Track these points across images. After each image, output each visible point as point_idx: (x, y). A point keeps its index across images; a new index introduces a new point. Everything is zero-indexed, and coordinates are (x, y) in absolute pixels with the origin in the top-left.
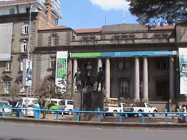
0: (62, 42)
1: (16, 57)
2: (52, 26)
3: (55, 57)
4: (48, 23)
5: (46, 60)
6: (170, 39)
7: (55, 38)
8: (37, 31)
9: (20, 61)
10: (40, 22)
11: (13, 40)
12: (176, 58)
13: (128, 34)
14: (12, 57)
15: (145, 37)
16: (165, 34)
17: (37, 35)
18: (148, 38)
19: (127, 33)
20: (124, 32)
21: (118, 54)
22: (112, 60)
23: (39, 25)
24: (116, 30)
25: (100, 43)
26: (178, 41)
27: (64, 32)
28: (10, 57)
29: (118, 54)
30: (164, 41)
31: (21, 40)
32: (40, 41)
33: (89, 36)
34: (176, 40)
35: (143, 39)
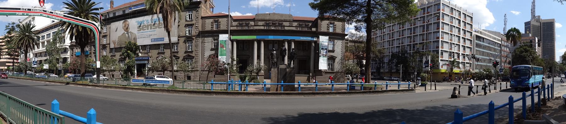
1: (182, 40)
2: (209, 13)
3: (218, 39)
5: (209, 43)
7: (216, 23)
8: (201, 18)
9: (186, 43)
10: (202, 10)
11: (179, 26)
12: (317, 44)
13: (277, 22)
14: (179, 40)
15: (291, 25)
16: (307, 24)
17: (200, 21)
18: (293, 26)
19: (277, 21)
20: (274, 20)
21: (271, 38)
22: (267, 43)
24: (268, 18)
25: (286, 28)
26: (319, 30)
29: (271, 38)
31: (187, 26)
32: (203, 25)
33: (244, 22)
34: (317, 30)
35: (289, 26)
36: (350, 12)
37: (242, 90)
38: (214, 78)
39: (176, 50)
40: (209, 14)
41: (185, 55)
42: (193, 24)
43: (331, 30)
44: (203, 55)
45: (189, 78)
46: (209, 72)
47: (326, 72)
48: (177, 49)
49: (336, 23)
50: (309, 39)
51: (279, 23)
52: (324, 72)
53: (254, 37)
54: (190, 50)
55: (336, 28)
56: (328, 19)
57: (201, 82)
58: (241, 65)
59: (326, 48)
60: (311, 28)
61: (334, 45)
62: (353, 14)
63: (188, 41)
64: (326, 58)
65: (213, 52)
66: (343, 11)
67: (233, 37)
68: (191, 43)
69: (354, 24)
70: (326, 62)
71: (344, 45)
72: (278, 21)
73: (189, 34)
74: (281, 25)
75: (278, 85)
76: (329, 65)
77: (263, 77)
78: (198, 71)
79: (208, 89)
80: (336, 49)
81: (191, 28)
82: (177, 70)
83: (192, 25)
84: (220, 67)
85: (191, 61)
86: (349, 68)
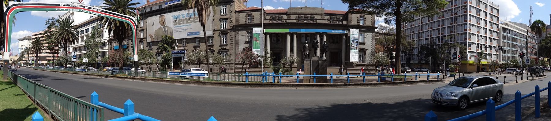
0: (256, 21)
1: (217, 33)
3: (251, 33)
4: (241, 5)
5: (243, 36)
6: (343, 22)
7: (250, 17)
9: (220, 37)
11: (213, 20)
14: (213, 34)
16: (338, 17)
17: (234, 15)
21: (303, 31)
22: (299, 36)
23: (236, 7)
24: (300, 12)
25: (318, 22)
26: (349, 24)
27: (258, 12)
28: (212, 34)
29: (303, 31)
30: (337, 23)
31: (221, 20)
32: (237, 19)
33: (277, 16)
34: (348, 23)
36: (379, 4)
37: (276, 82)
38: (249, 70)
39: (211, 44)
40: (243, 8)
41: (220, 48)
42: (228, 18)
43: (361, 23)
44: (237, 48)
45: (224, 71)
46: (244, 65)
47: (357, 64)
48: (212, 43)
49: (366, 16)
50: (340, 32)
51: (311, 17)
52: (355, 64)
53: (287, 30)
54: (225, 43)
55: (366, 21)
56: (358, 12)
57: (236, 75)
58: (274, 57)
59: (357, 40)
60: (342, 21)
61: (364, 37)
62: (382, 7)
63: (222, 34)
64: (357, 51)
65: (247, 45)
66: (373, 4)
67: (266, 31)
68: (225, 37)
69: (384, 17)
70: (357, 54)
71: (375, 37)
72: (310, 15)
73: (224, 28)
74: (313, 19)
75: (310, 77)
76: (360, 57)
77: (296, 69)
78: (233, 63)
79: (242, 81)
80: (366, 41)
81: (225, 22)
82: (212, 63)
83: (226, 19)
84: (254, 60)
85: (226, 54)
86: (379, 60)
